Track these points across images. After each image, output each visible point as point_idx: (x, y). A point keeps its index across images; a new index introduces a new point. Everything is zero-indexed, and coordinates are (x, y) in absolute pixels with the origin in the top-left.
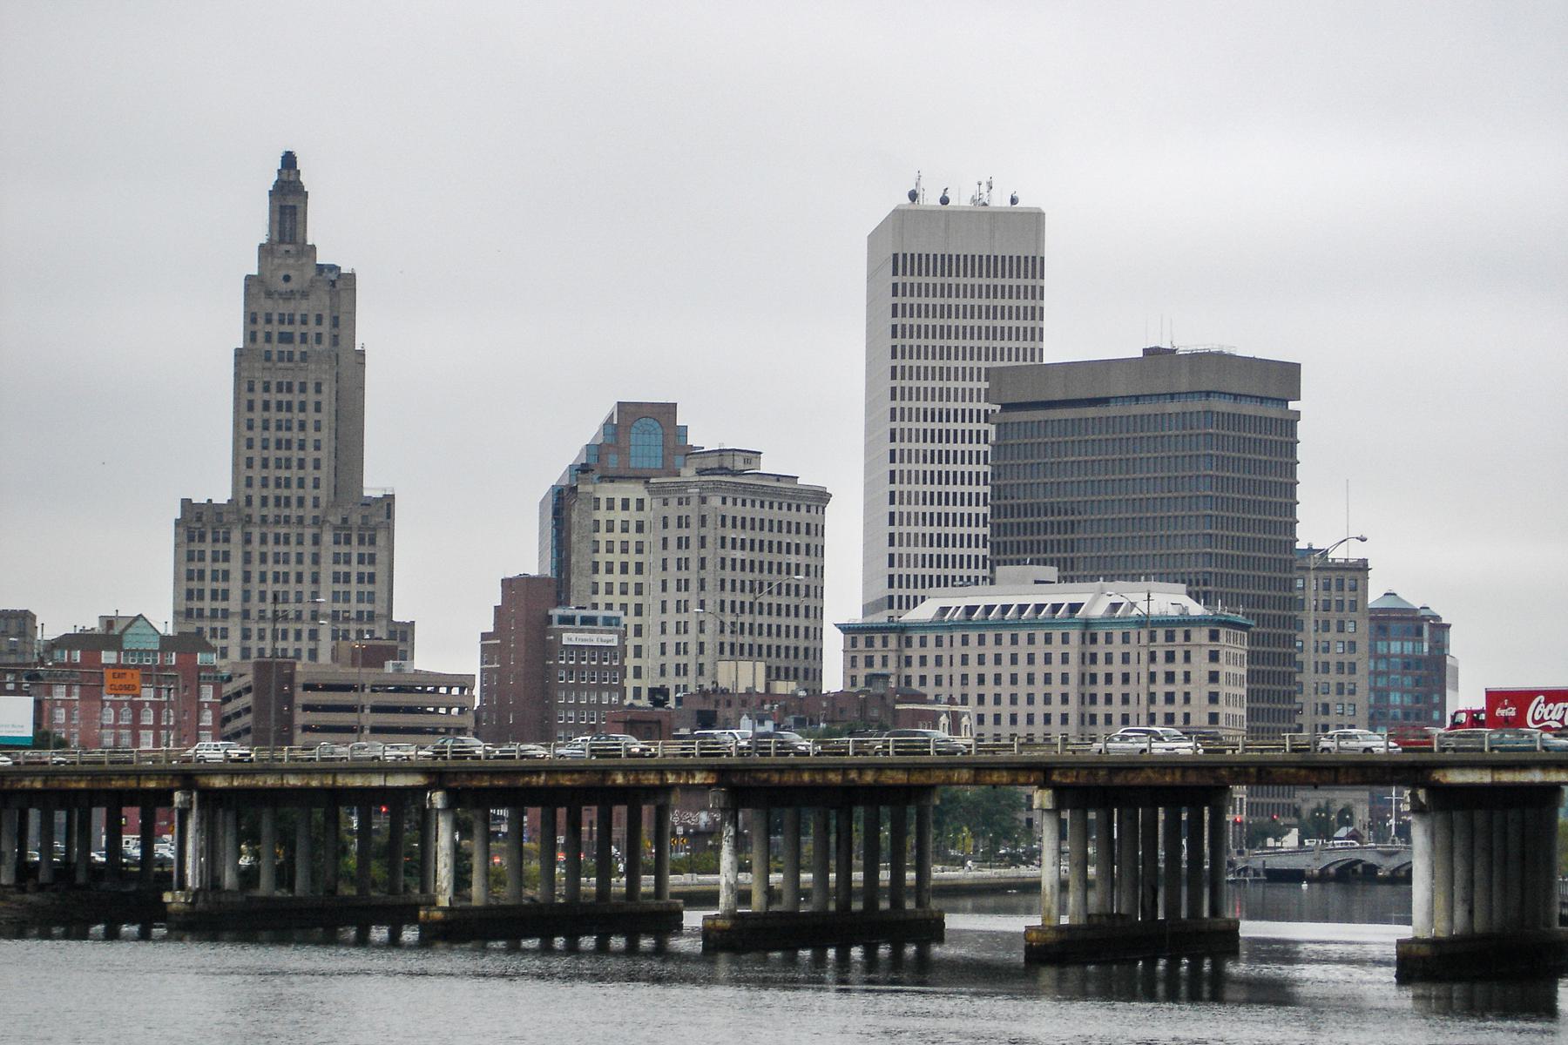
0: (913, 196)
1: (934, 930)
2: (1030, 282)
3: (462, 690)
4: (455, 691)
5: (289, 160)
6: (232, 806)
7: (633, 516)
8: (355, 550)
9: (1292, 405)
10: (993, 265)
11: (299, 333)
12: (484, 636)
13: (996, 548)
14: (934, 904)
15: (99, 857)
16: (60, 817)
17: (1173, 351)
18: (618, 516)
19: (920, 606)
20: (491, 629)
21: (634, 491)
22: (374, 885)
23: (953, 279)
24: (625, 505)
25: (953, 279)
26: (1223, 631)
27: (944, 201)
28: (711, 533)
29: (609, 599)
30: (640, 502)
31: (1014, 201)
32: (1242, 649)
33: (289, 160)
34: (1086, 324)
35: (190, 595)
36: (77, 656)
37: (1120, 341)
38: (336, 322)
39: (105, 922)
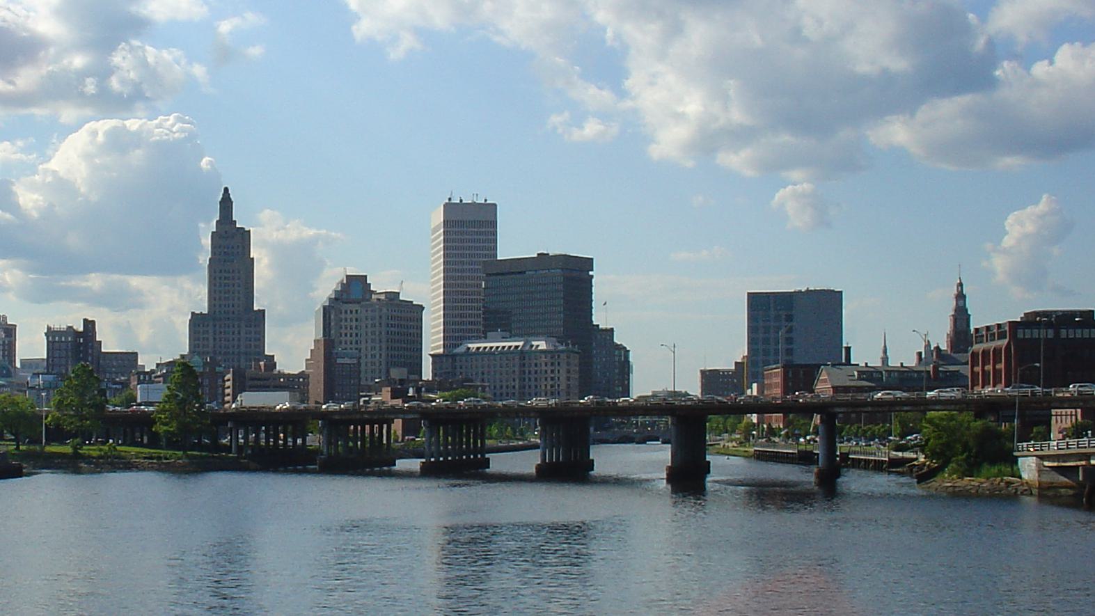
0: (450, 199)
1: (486, 463)
2: (492, 230)
3: (304, 379)
4: (301, 380)
5: (226, 190)
6: (334, 424)
7: (354, 316)
8: (252, 329)
9: (591, 273)
10: (480, 224)
11: (231, 251)
12: (307, 360)
13: (485, 326)
14: (487, 456)
15: (263, 444)
16: (290, 427)
17: (548, 254)
18: (349, 316)
19: (460, 347)
20: (309, 357)
21: (354, 307)
22: (801, 445)
23: (469, 228)
24: (351, 312)
25: (469, 228)
26: (572, 355)
27: (461, 201)
28: (384, 321)
29: (351, 346)
30: (357, 311)
31: (486, 200)
32: (577, 361)
33: (226, 190)
34: (513, 244)
35: (195, 346)
36: (916, 375)
37: (529, 251)
38: (244, 248)
39: (1013, 455)
